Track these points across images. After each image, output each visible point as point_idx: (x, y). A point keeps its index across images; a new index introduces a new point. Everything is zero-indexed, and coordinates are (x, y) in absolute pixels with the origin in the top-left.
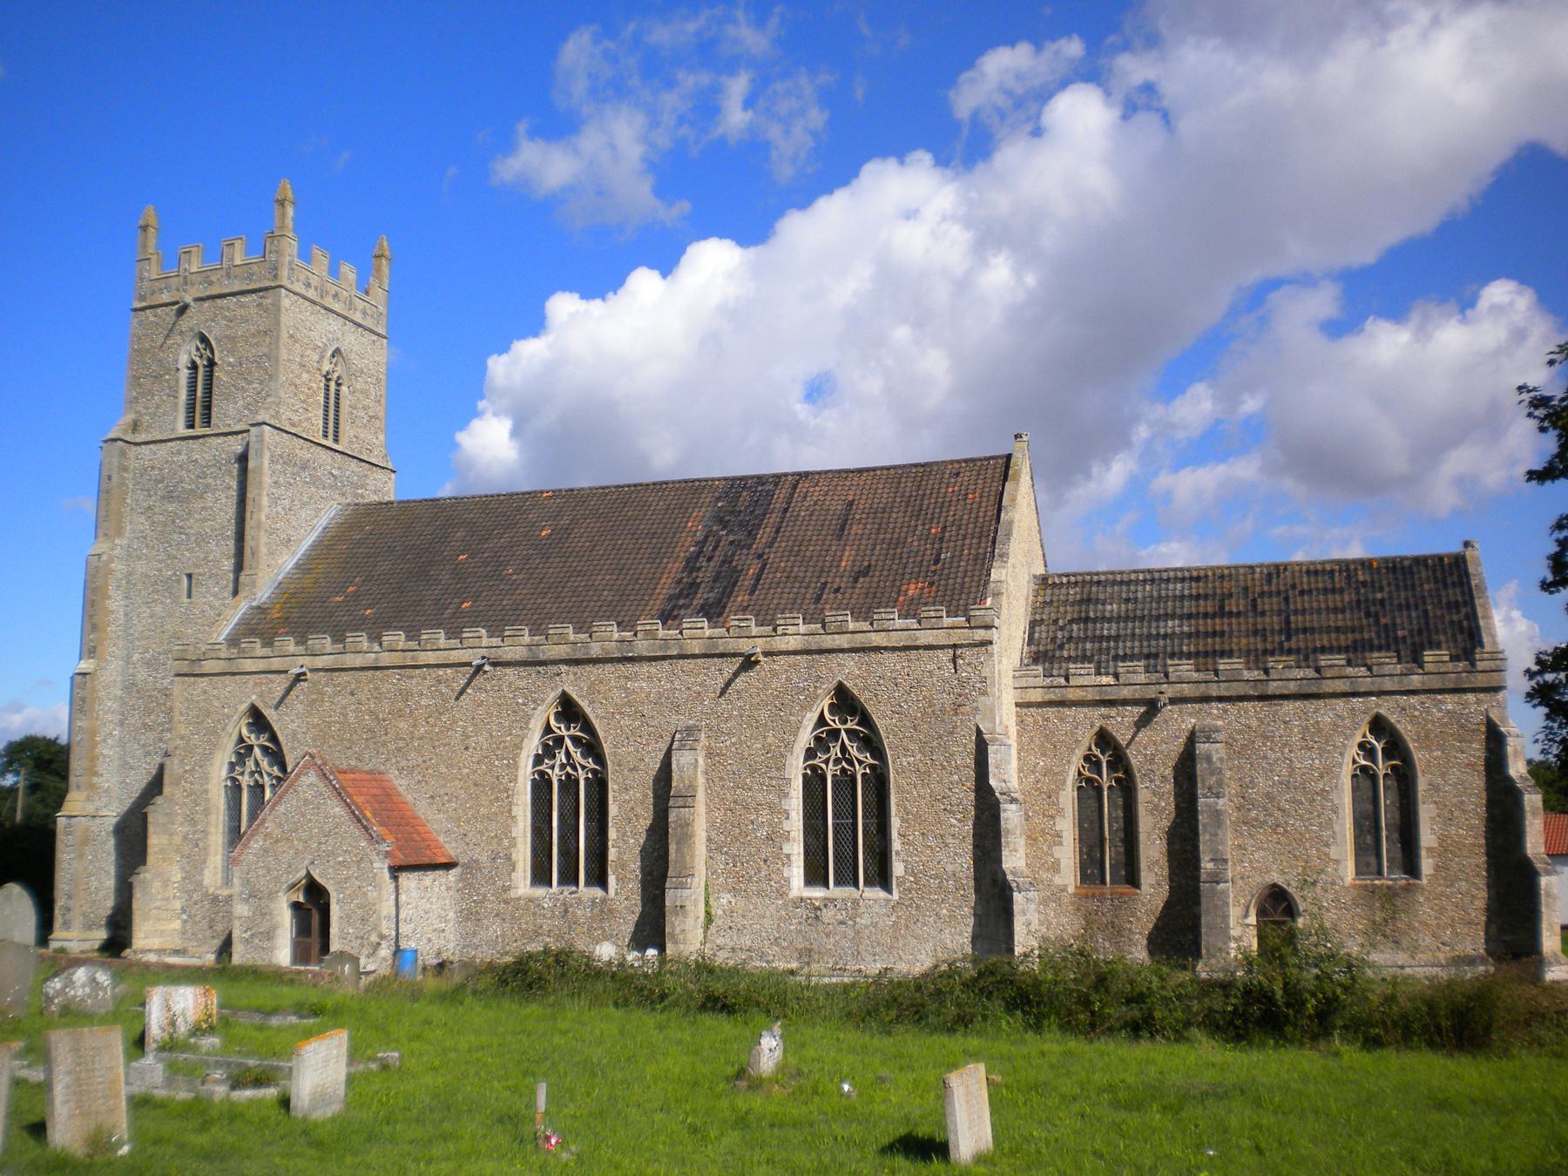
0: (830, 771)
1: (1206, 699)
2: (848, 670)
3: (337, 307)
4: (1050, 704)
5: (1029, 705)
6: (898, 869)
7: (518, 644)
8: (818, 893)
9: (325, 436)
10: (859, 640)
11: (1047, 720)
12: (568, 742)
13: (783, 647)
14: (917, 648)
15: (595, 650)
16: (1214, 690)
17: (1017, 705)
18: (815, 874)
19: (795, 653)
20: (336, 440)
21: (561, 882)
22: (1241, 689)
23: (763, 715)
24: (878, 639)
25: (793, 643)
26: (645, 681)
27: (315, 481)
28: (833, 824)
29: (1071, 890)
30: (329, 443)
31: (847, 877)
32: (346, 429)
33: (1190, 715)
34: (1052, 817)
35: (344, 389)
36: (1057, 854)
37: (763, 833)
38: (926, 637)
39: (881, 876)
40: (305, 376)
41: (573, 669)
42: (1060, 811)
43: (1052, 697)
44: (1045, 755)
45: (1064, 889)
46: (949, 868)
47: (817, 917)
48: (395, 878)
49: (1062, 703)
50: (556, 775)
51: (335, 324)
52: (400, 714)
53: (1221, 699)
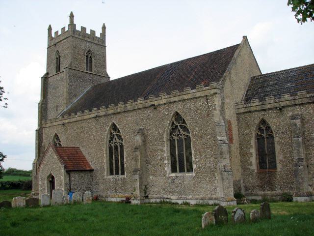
0: (176, 138)
1: (295, 105)
2: (178, 108)
3: (89, 40)
4: (246, 112)
5: (240, 113)
6: (194, 166)
7: (102, 112)
8: (173, 175)
9: (87, 70)
10: (180, 98)
11: (246, 118)
12: (115, 136)
13: (162, 103)
14: (196, 98)
15: (119, 110)
16: (297, 102)
17: (237, 114)
18: (174, 170)
19: (165, 104)
20: (91, 71)
21: (116, 174)
22: (306, 101)
23: (157, 123)
24: (185, 97)
25: (164, 101)
26: (131, 118)
27: (83, 81)
28: (178, 154)
29: (256, 171)
30: (89, 72)
31: (182, 170)
32: (94, 68)
33: (290, 111)
34: (249, 148)
35: (93, 59)
36: (251, 160)
37: (159, 158)
38: (198, 95)
39: (190, 169)
40: (79, 56)
41: (115, 116)
42: (251, 146)
43: (246, 110)
44: (246, 129)
45: (254, 171)
46: (208, 165)
47: (174, 182)
48: (69, 174)
49: (250, 112)
50: (113, 145)
51: (89, 44)
52: (81, 132)
53: (299, 105)
